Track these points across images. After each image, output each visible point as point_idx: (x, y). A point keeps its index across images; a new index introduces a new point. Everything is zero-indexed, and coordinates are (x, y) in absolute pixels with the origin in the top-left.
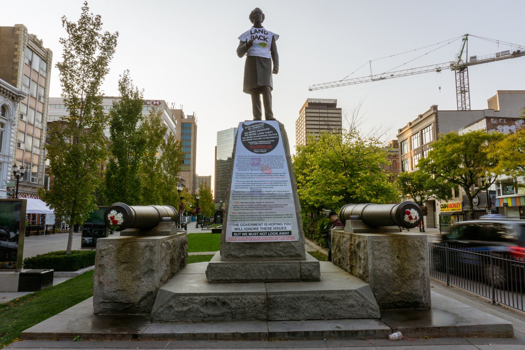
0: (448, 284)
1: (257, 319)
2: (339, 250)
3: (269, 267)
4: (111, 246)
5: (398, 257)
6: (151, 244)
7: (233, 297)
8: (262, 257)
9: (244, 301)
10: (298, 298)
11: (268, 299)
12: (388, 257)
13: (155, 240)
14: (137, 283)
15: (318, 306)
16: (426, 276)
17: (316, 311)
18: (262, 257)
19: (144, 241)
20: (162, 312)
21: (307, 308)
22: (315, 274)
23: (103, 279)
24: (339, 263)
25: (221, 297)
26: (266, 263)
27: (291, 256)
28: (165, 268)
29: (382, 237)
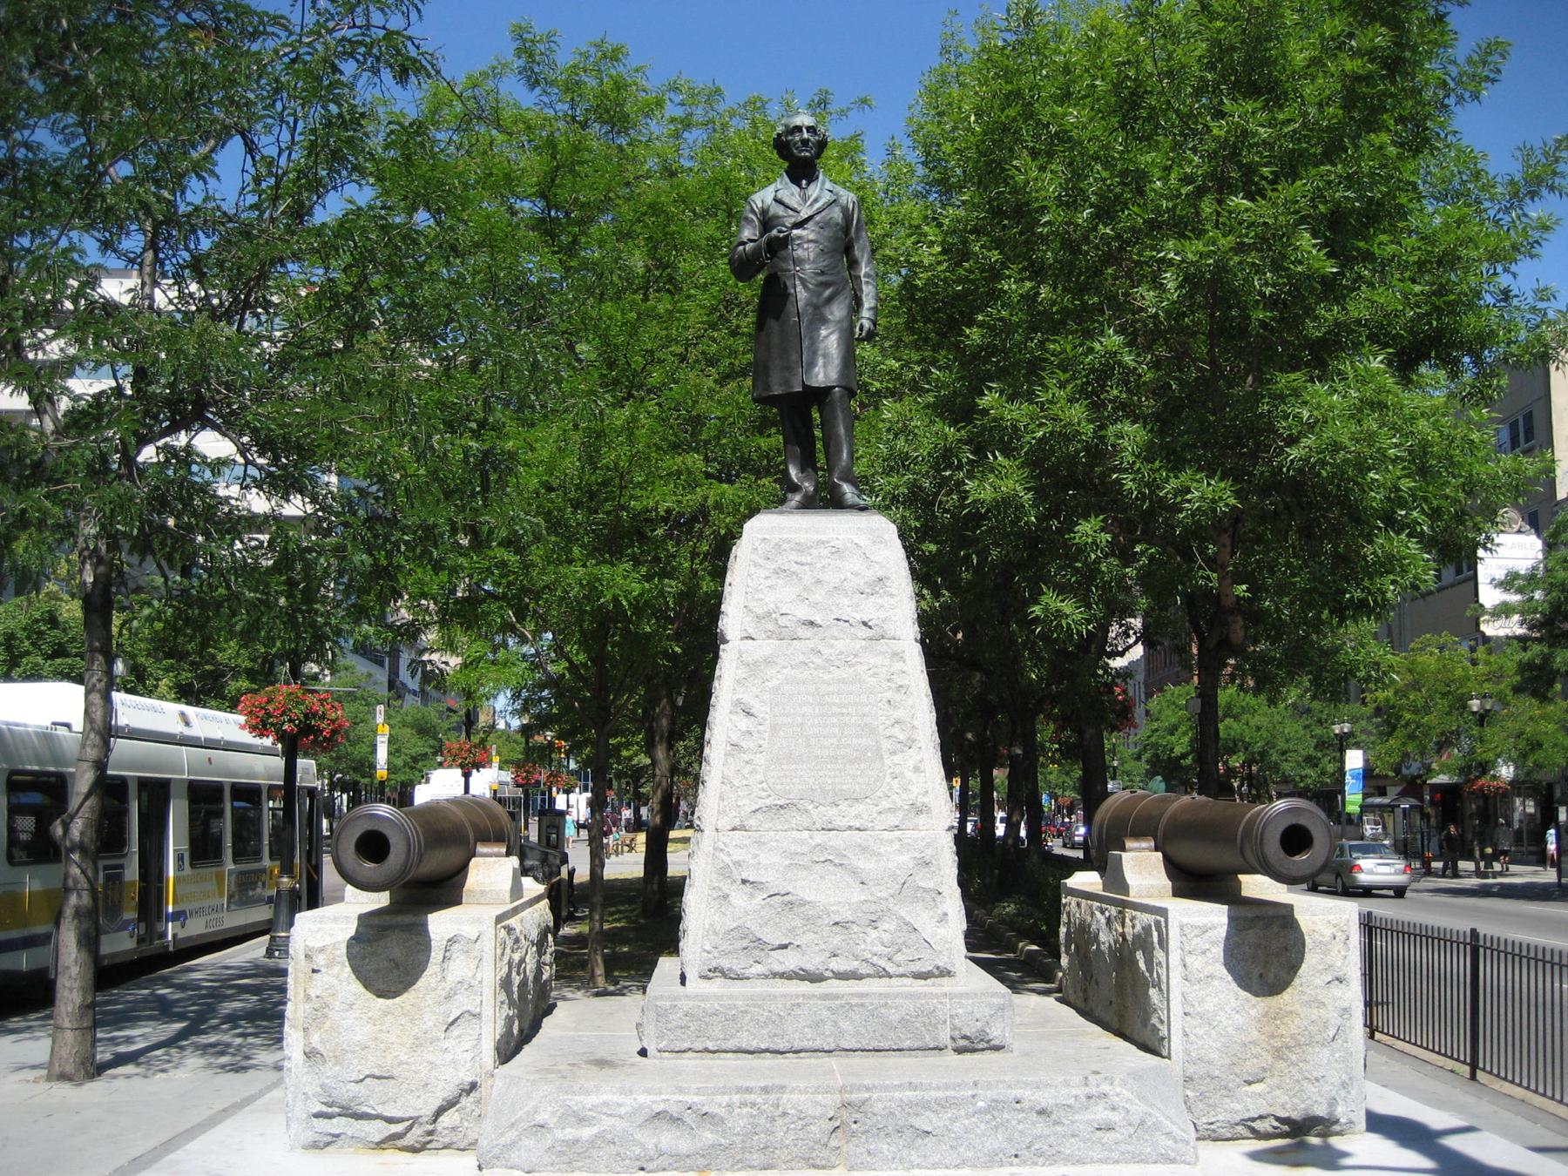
0: (1473, 1077)
15: (1004, 1125)
20: (513, 1143)
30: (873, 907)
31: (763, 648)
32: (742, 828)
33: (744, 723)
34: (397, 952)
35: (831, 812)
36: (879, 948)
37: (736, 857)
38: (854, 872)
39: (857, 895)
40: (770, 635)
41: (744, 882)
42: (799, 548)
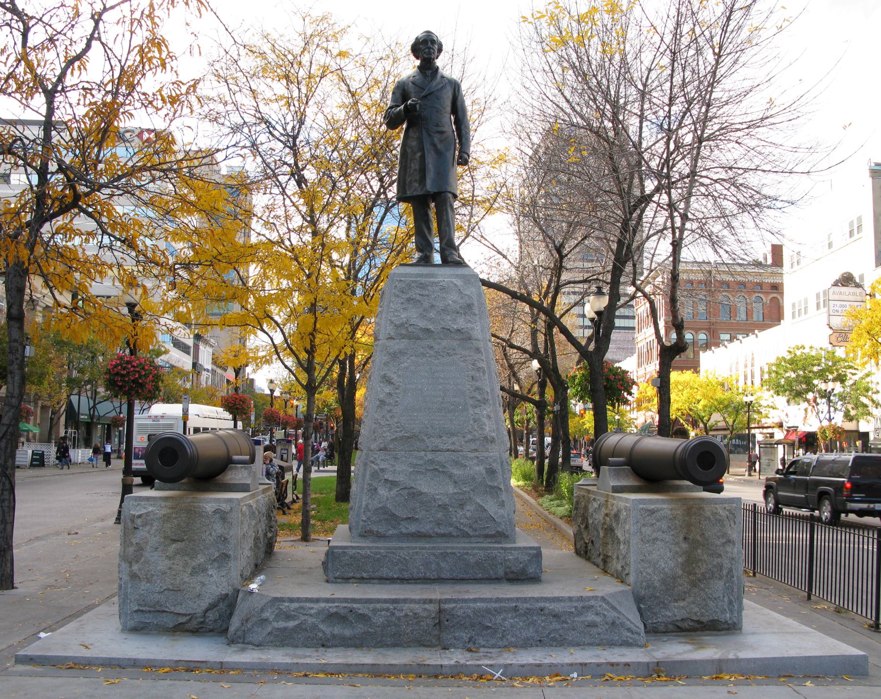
1: (421, 643)
2: (587, 527)
3: (444, 556)
4: (151, 509)
5: (685, 538)
6: (225, 507)
7: (378, 606)
8: (430, 536)
9: (398, 614)
10: (498, 611)
11: (440, 611)
12: (668, 537)
13: (230, 500)
14: (200, 578)
15: (533, 623)
16: (735, 574)
17: (530, 632)
18: (430, 536)
19: (212, 501)
21: (512, 626)
22: (531, 570)
23: (140, 569)
24: (586, 552)
25: (355, 606)
26: (439, 549)
27: (487, 536)
28: (247, 553)
29: (658, 500)
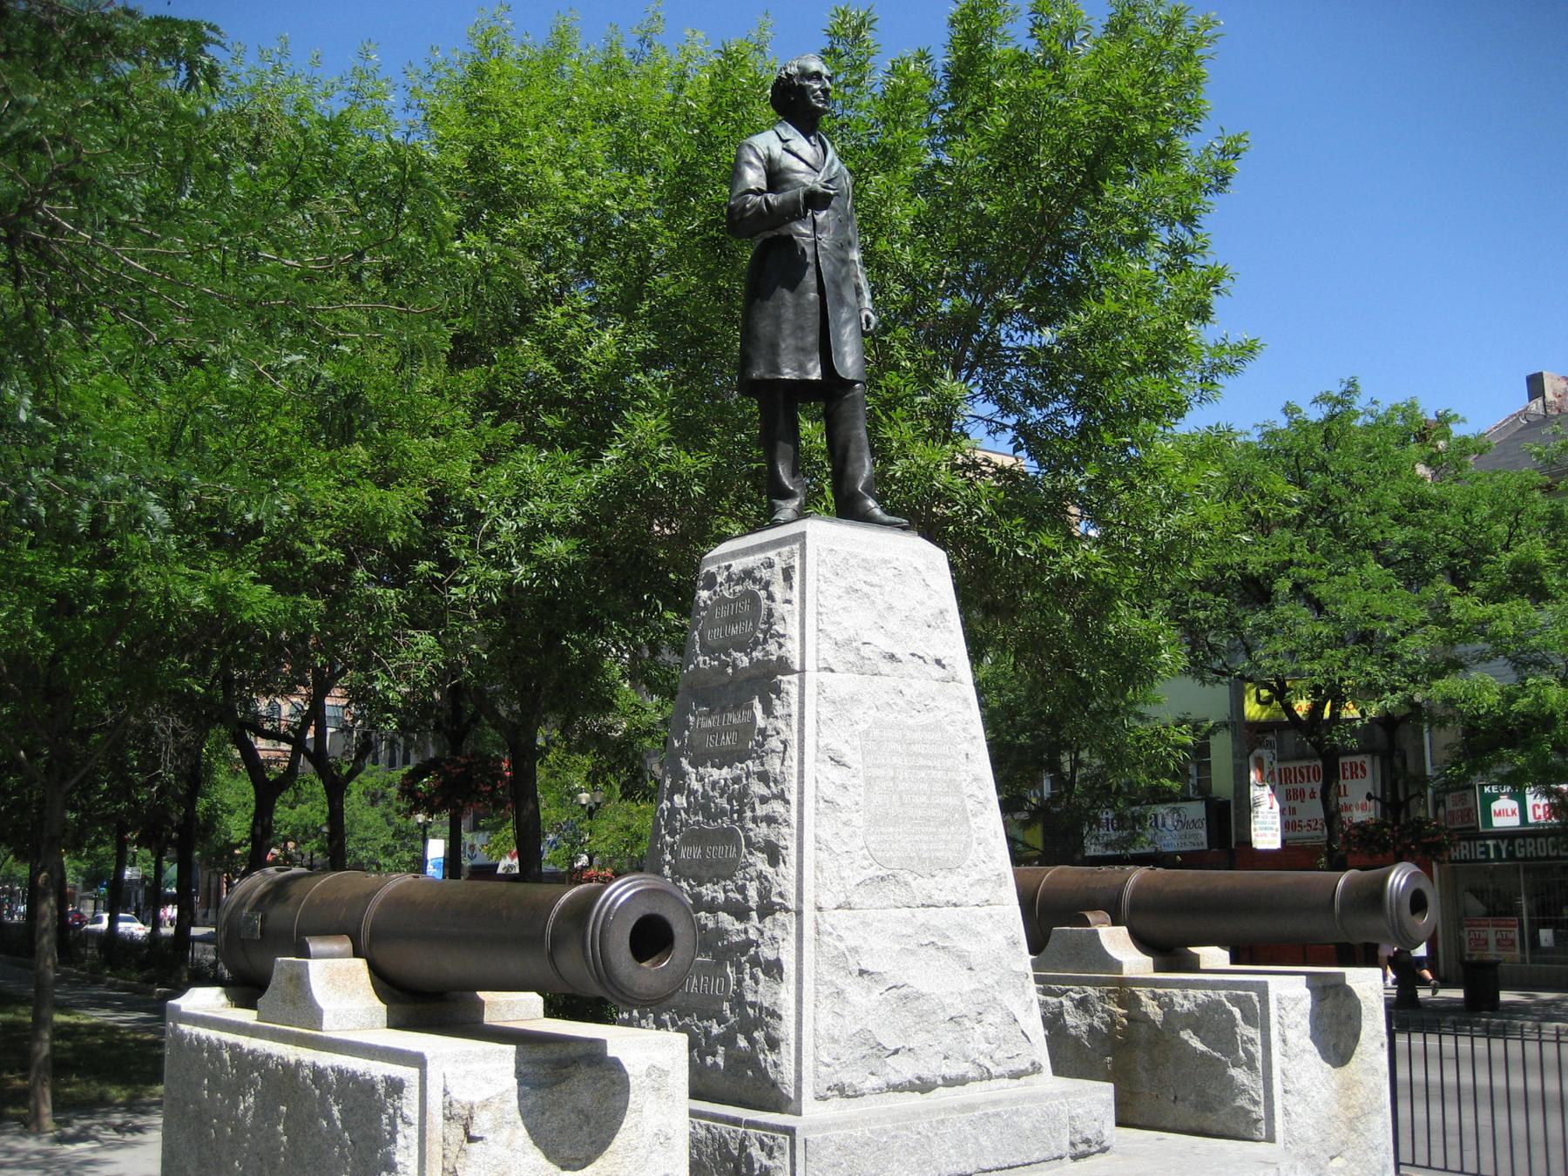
30: (982, 997)
31: (843, 683)
32: (848, 906)
33: (836, 774)
34: (586, 1099)
35: (929, 884)
36: (984, 1046)
37: (852, 943)
38: (960, 956)
39: (967, 983)
40: (850, 667)
41: (862, 972)
42: (867, 565)
